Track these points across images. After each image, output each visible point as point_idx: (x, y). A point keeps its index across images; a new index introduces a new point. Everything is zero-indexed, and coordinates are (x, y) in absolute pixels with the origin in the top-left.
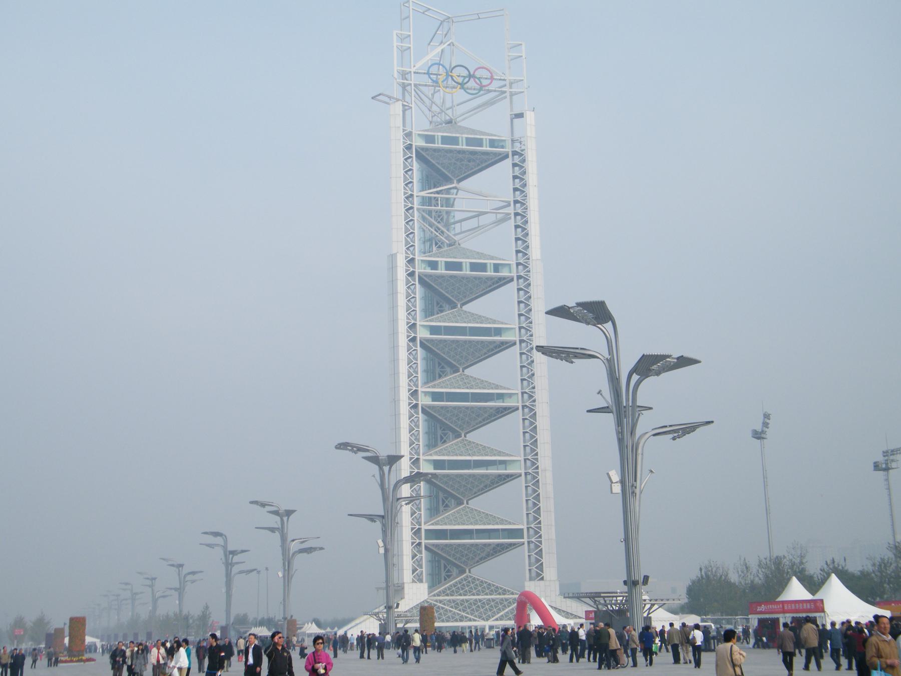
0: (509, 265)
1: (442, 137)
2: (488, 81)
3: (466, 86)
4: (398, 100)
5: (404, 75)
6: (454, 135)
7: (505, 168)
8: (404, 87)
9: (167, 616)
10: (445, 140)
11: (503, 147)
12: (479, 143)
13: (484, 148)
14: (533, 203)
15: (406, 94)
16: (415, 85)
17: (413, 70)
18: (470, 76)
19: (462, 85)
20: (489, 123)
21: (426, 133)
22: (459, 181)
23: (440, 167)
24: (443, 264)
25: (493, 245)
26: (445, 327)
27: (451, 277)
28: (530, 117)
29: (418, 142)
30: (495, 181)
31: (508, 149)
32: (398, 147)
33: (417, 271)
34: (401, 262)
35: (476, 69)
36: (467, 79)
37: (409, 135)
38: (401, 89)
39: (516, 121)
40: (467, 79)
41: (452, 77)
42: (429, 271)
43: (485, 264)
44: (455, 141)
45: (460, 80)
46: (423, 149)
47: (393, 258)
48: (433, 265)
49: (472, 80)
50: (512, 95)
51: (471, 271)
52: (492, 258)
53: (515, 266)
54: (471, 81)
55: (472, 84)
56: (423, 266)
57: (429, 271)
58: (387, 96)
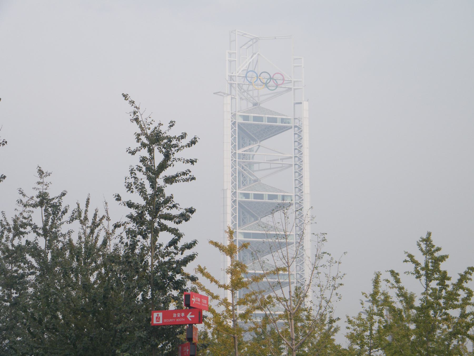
0: (291, 196)
1: (254, 117)
2: (281, 82)
3: (268, 85)
4: (228, 95)
5: (231, 77)
6: (260, 115)
7: (289, 135)
8: (231, 85)
9: (414, 300)
10: (255, 119)
11: (289, 123)
12: (275, 120)
13: (278, 124)
14: (306, 159)
15: (232, 89)
16: (238, 84)
17: (237, 74)
18: (271, 78)
19: (266, 84)
20: (277, 106)
21: (244, 114)
22: (260, 141)
23: (253, 136)
24: (267, 196)
25: (279, 183)
26: (253, 233)
27: (257, 203)
28: (306, 105)
29: (240, 120)
30: (281, 144)
31: (292, 124)
32: (228, 124)
33: (237, 199)
34: (229, 194)
35: (274, 75)
36: (269, 80)
37: (234, 115)
38: (229, 85)
39: (296, 105)
40: (269, 80)
41: (260, 79)
42: (244, 199)
43: (262, 195)
44: (260, 119)
45: (264, 81)
46: (242, 124)
47: (224, 191)
48: (247, 196)
49: (272, 80)
50: (295, 89)
51: (269, 199)
52: (281, 191)
53: (294, 196)
54: (271, 82)
55: (272, 83)
56: (241, 196)
57: (244, 199)
58: (223, 93)
